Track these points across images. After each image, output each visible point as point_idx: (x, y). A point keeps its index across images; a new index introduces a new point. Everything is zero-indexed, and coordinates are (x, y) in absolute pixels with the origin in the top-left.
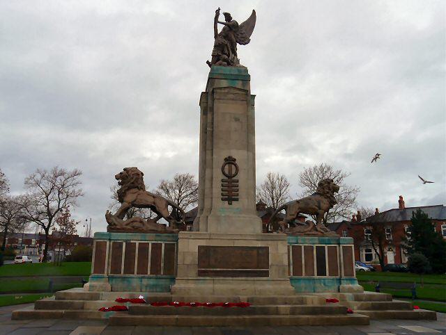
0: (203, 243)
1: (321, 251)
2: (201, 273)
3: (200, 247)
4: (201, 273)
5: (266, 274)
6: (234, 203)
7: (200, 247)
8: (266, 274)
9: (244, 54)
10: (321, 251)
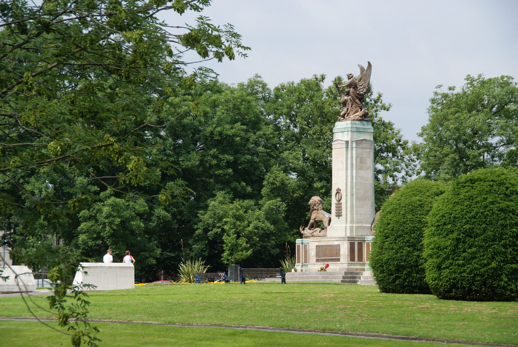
0: (318, 244)
2: (317, 261)
3: (317, 246)
4: (317, 261)
5: (338, 260)
6: (340, 217)
7: (317, 246)
8: (338, 260)
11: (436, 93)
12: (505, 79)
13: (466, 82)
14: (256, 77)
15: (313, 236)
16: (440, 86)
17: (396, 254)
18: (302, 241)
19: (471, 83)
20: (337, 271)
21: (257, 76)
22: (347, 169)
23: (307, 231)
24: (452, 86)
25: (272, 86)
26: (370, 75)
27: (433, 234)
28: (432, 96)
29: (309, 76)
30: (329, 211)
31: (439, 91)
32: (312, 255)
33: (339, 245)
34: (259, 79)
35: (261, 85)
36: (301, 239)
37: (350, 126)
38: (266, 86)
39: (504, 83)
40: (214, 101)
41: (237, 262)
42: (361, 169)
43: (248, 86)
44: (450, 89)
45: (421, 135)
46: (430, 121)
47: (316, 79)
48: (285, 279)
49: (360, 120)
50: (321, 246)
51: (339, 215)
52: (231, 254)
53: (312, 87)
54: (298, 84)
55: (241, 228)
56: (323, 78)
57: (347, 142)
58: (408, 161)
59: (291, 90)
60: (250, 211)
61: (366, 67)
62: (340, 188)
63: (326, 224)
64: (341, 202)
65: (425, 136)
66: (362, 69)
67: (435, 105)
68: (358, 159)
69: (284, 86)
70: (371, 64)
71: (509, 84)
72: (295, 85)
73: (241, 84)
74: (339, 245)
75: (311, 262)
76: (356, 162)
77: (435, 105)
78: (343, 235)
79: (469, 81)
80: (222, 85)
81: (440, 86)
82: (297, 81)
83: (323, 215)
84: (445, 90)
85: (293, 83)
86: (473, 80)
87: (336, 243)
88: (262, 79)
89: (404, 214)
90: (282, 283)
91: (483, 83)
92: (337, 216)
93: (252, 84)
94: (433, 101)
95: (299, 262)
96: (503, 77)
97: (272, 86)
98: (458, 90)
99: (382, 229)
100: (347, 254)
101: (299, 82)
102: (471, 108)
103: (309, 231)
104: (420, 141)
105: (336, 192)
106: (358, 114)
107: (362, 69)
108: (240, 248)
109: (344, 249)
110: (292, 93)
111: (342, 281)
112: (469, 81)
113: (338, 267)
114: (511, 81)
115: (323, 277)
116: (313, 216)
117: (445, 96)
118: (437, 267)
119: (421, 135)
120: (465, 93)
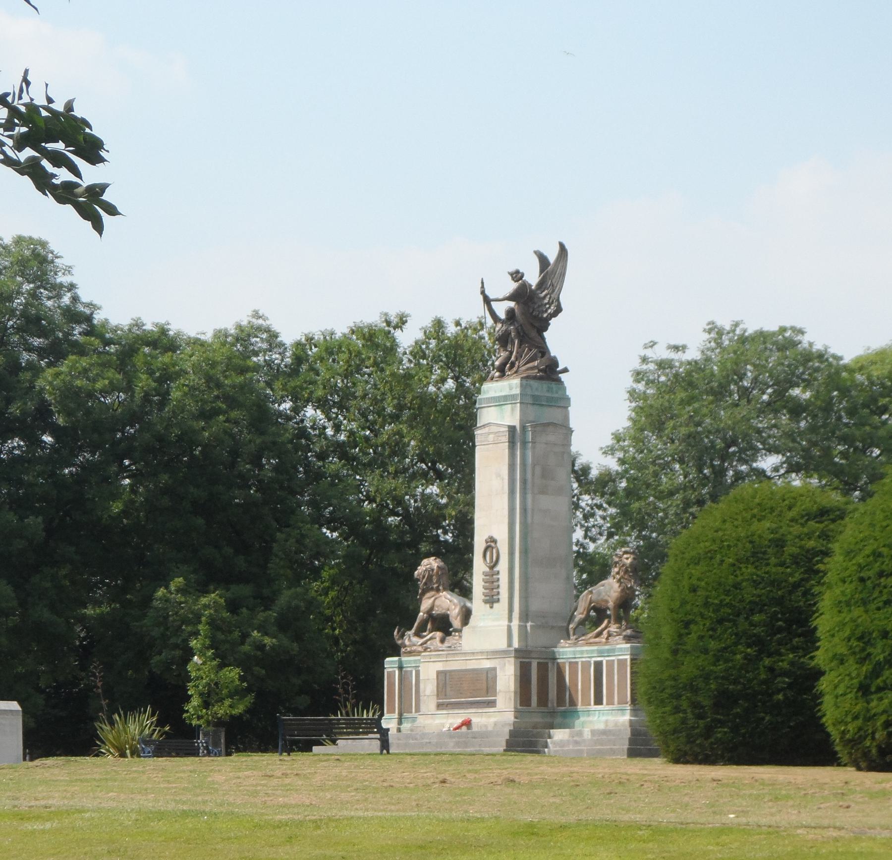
0: (440, 667)
1: (598, 665)
2: (440, 706)
3: (439, 673)
4: (440, 706)
5: (492, 704)
6: (495, 605)
7: (439, 673)
8: (492, 704)
9: (556, 338)
10: (598, 665)
11: (644, 360)
12: (787, 334)
13: (706, 336)
14: (253, 316)
15: (425, 650)
16: (653, 344)
17: (715, 665)
18: (400, 662)
19: (718, 342)
20: (490, 729)
21: (257, 315)
22: (512, 492)
23: (410, 639)
24: (679, 343)
25: (289, 336)
26: (563, 275)
27: (848, 604)
28: (637, 365)
29: (371, 317)
30: (466, 592)
31: (649, 353)
32: (428, 692)
33: (495, 669)
34: (260, 322)
35: (264, 336)
36: (396, 659)
37: (517, 391)
38: (277, 337)
39: (784, 342)
40: (165, 369)
41: (219, 723)
42: (543, 491)
43: (237, 339)
44: (676, 348)
45: (610, 451)
46: (630, 419)
47: (388, 323)
48: (387, 741)
49: (541, 378)
50: (450, 671)
51: (491, 600)
52: (206, 705)
53: (376, 342)
54: (344, 335)
55: (227, 646)
56: (402, 321)
57: (512, 429)
58: (588, 508)
59: (331, 348)
60: (244, 610)
61: (552, 257)
62: (496, 537)
63: (456, 623)
64: (496, 569)
65: (620, 455)
66: (543, 260)
67: (641, 387)
68: (538, 470)
69: (312, 339)
70: (567, 247)
71: (794, 344)
72: (338, 335)
73: (220, 331)
74: (495, 669)
75: (423, 708)
76: (533, 475)
77: (641, 387)
78: (502, 645)
79: (712, 335)
80: (178, 334)
81: (653, 344)
82: (341, 329)
83: (446, 602)
84: (662, 353)
85: (332, 333)
86: (720, 333)
87: (487, 664)
88: (268, 322)
89: (734, 565)
90: (381, 753)
91: (743, 340)
92: (486, 602)
93: (244, 336)
94: (639, 376)
95: (391, 711)
96: (783, 330)
97: (289, 336)
98: (693, 354)
99: (678, 604)
100: (512, 688)
101: (347, 331)
102: (719, 393)
103: (415, 639)
104: (612, 464)
105: (484, 545)
106: (536, 363)
107: (543, 260)
108: (225, 692)
109: (507, 677)
110: (331, 353)
111: (505, 750)
112: (712, 335)
113: (493, 720)
114: (799, 337)
115: (457, 744)
116: (425, 605)
117: (663, 365)
118: (859, 689)
119: (610, 451)
120: (708, 360)
